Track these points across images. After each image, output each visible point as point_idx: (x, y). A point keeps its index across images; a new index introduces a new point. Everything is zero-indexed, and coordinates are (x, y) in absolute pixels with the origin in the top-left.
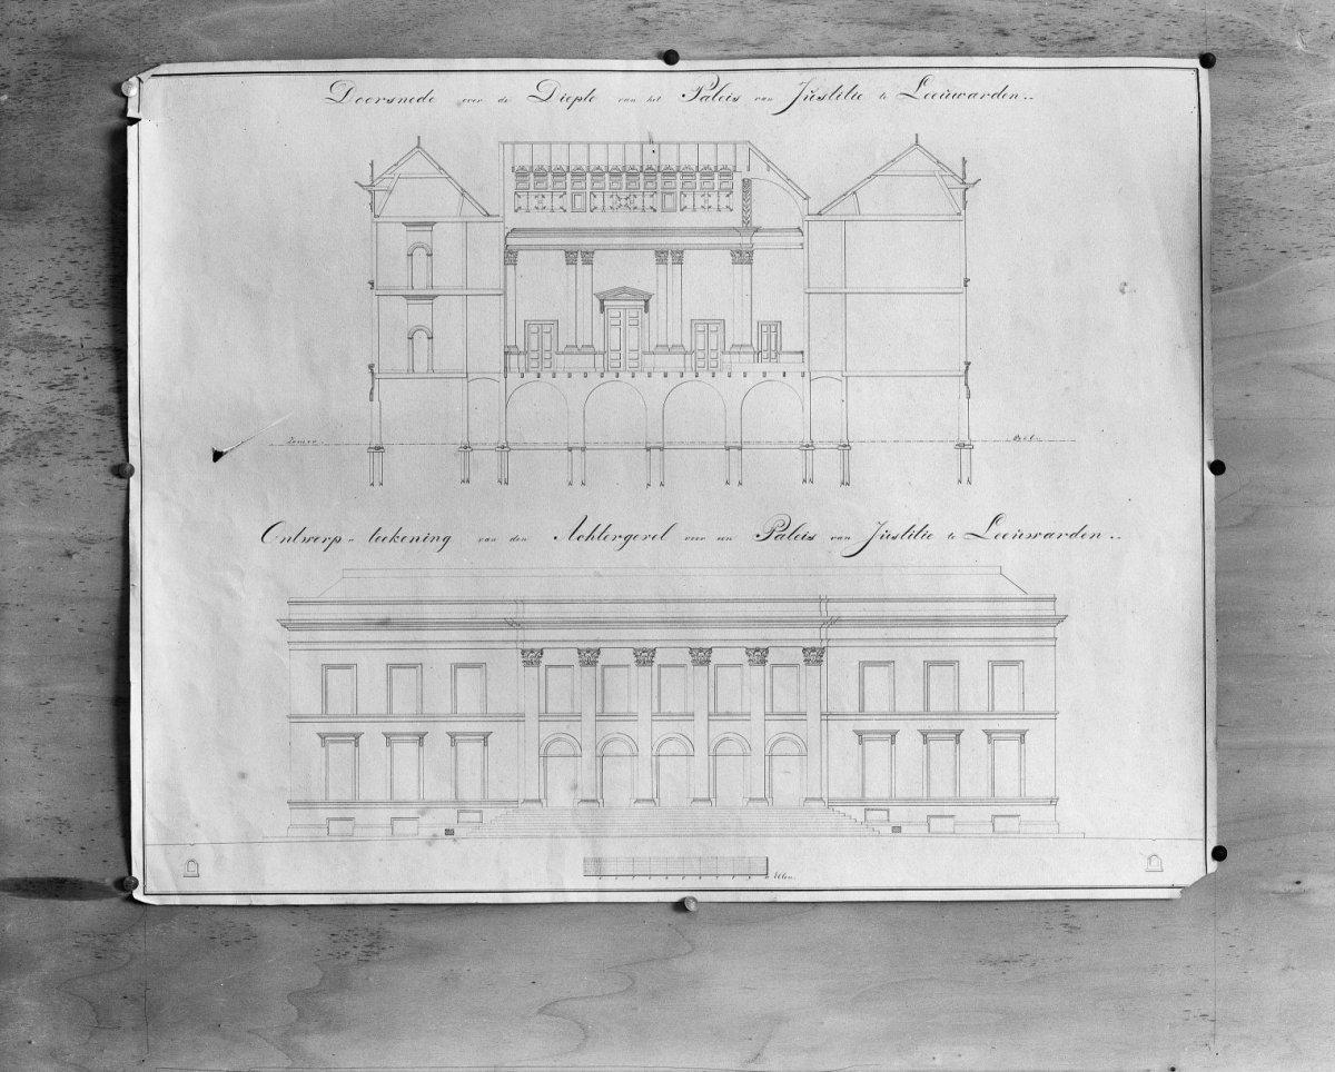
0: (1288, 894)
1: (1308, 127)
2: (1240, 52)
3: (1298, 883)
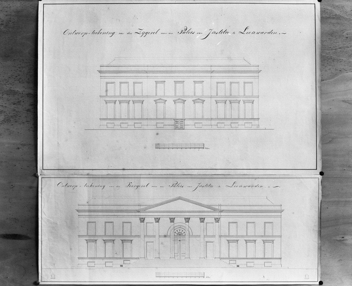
0: (340, 241)
1: (347, 38)
2: (329, 17)
3: (343, 238)
